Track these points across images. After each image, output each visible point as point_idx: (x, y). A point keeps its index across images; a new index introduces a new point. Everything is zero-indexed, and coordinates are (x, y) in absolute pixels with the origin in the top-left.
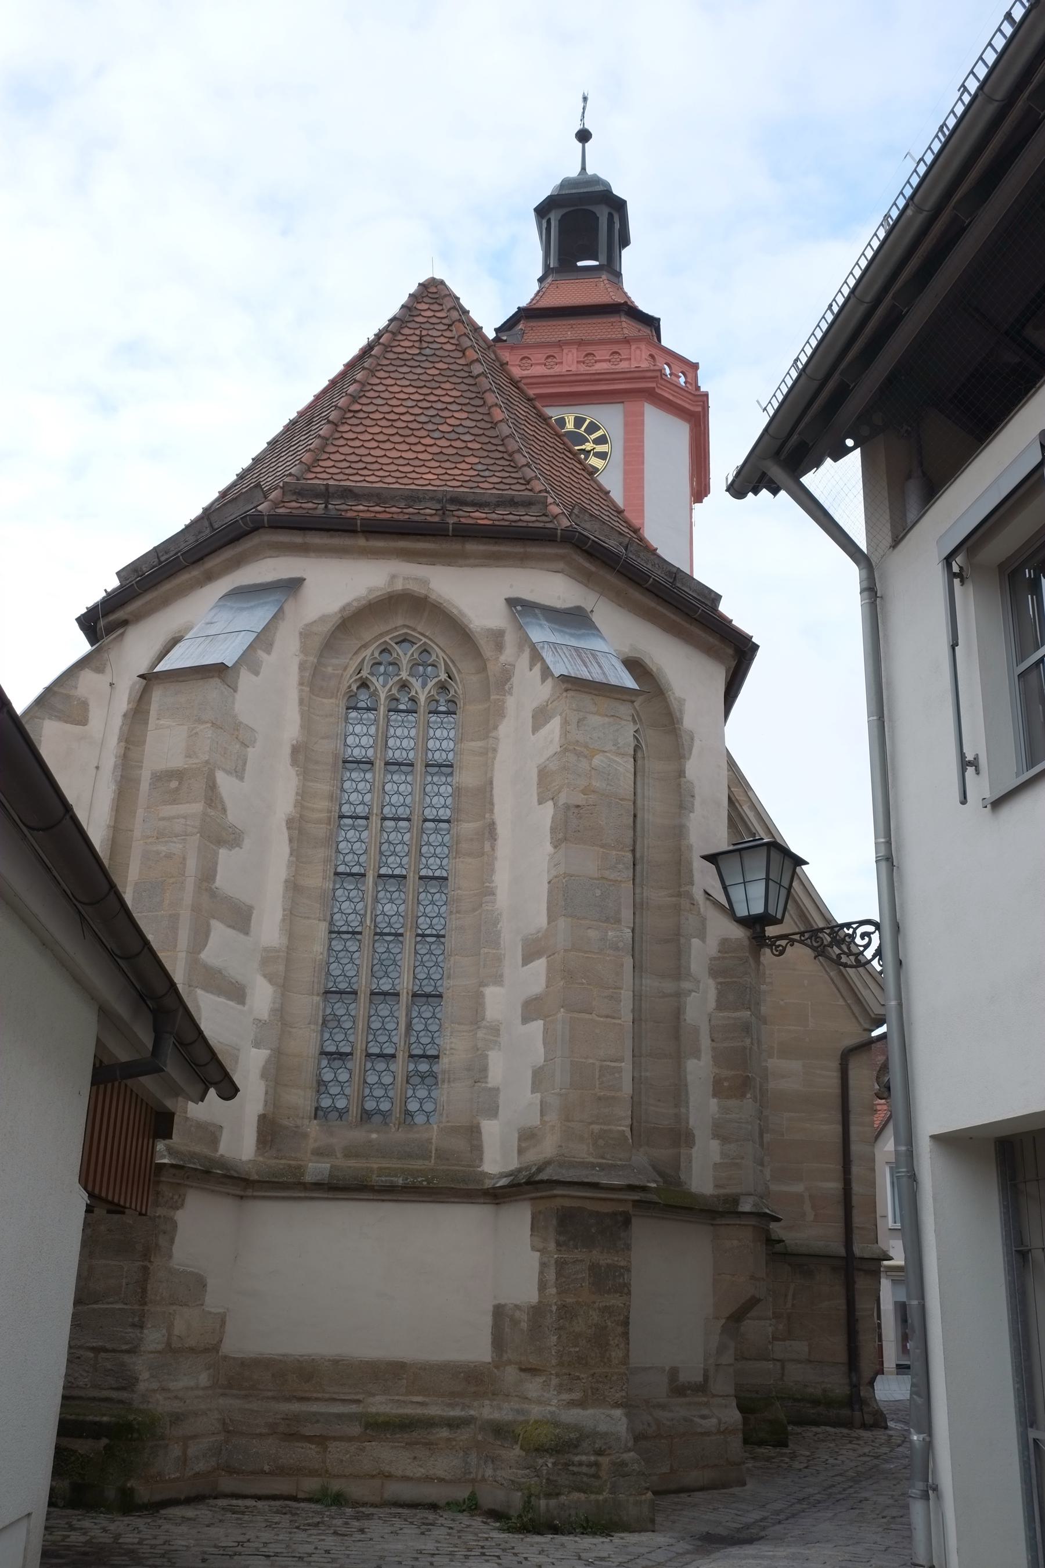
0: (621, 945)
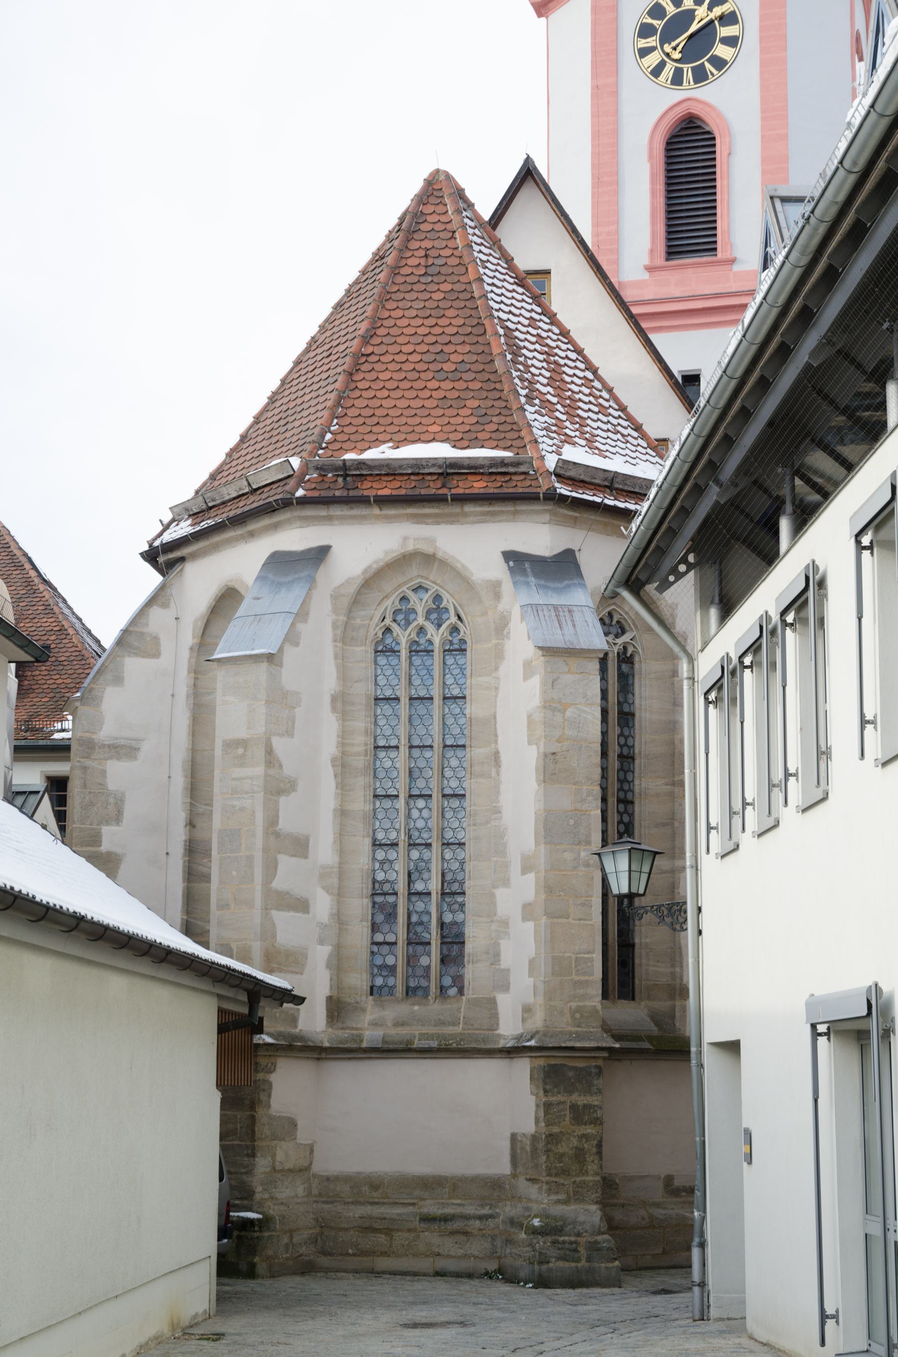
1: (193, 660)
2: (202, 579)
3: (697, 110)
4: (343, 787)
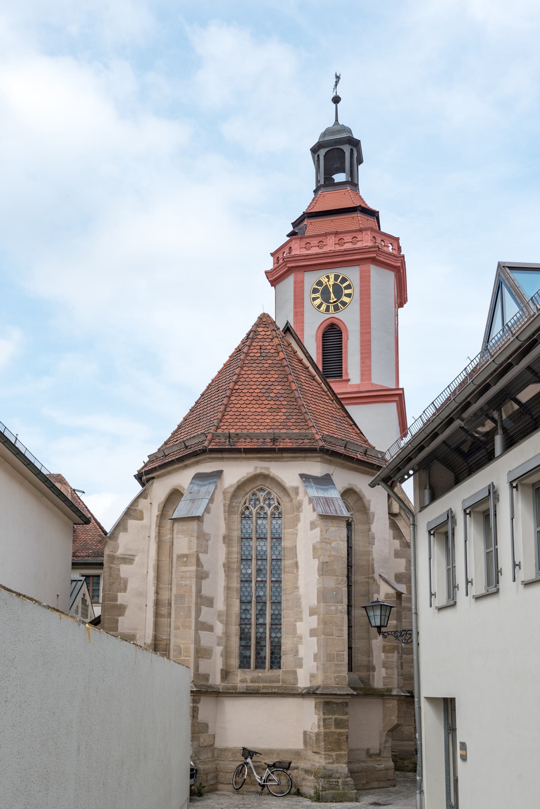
0: (343, 611)
1: (158, 522)
2: (161, 489)
3: (336, 322)
4: (228, 577)
